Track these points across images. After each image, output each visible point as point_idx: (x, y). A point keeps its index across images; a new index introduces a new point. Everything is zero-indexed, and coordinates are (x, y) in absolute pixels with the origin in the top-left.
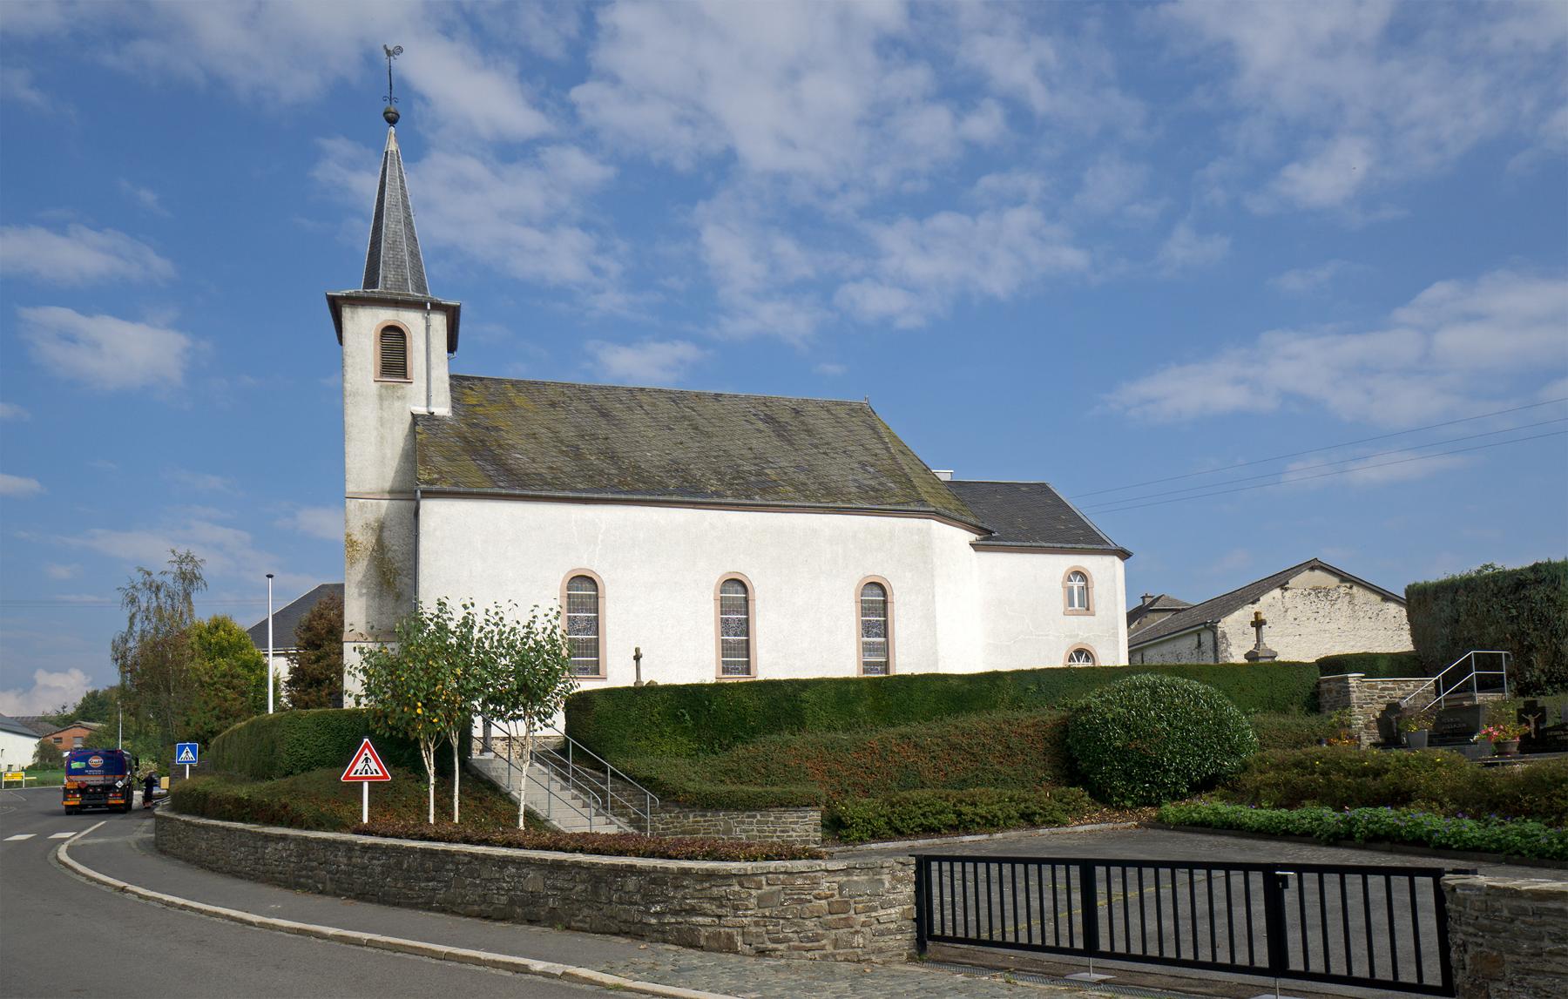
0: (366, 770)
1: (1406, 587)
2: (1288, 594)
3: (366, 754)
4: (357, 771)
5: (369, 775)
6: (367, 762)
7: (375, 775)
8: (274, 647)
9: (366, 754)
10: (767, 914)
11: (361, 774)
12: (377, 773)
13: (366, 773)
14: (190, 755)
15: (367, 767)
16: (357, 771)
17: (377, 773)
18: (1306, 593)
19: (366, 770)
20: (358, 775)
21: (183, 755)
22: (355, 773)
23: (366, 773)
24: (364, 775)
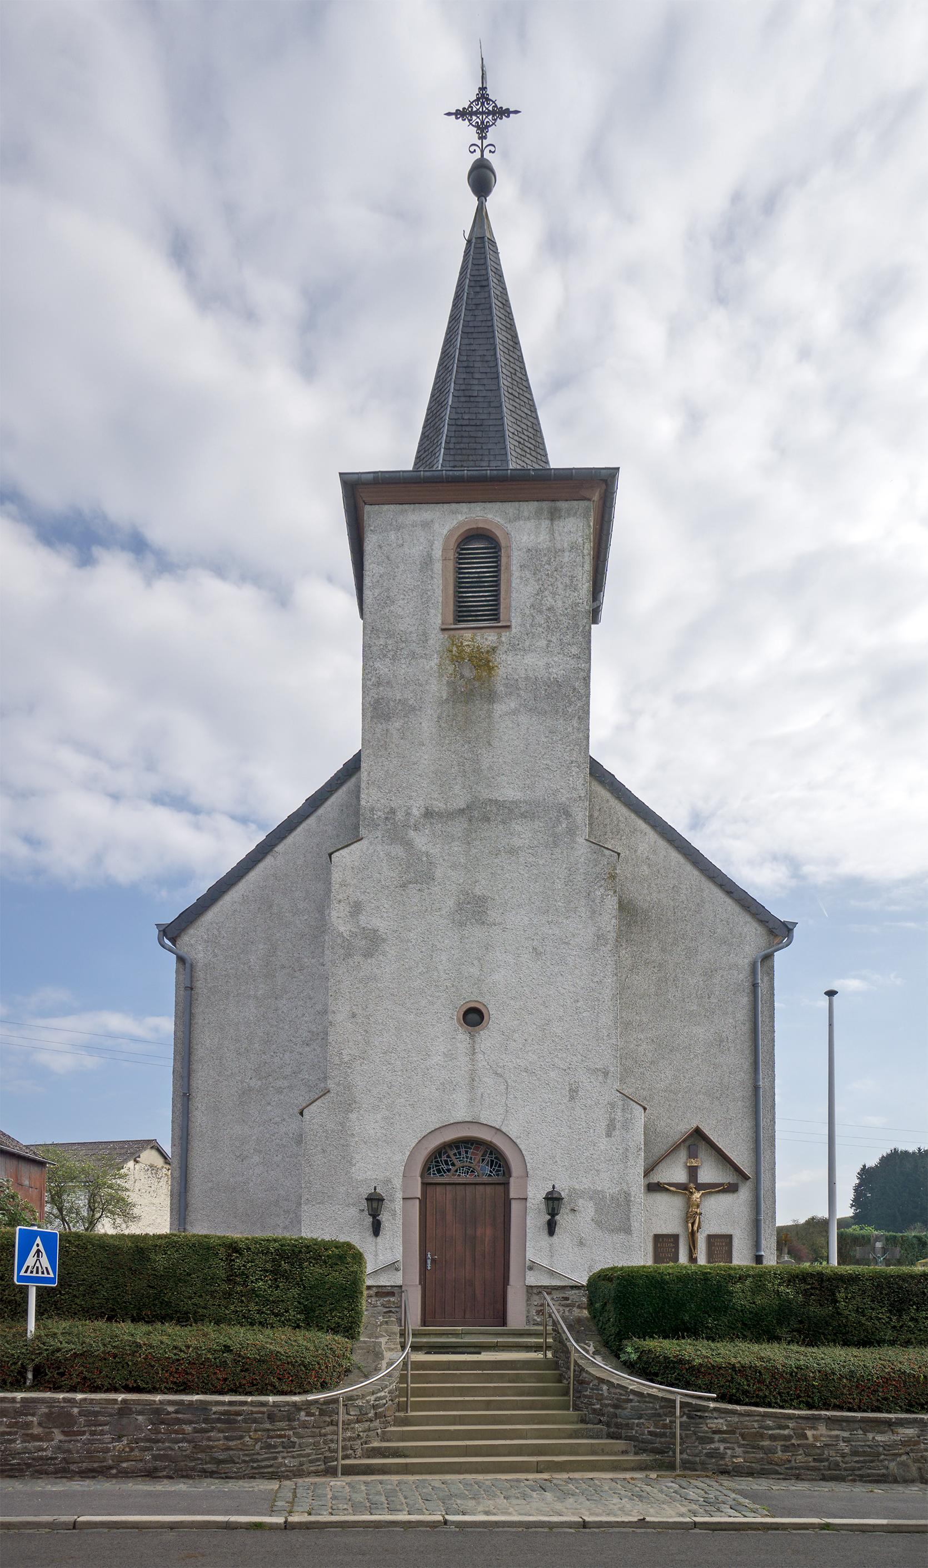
0: (37, 1268)
1: (893, 1148)
2: (137, 1166)
3: (38, 1245)
4: (28, 1267)
5: (40, 1275)
6: (38, 1256)
7: (46, 1275)
8: (40, 1313)
9: (38, 1245)
10: (305, 1342)
11: (32, 1272)
12: (48, 1273)
13: (37, 1272)
14: (45, 1261)
15: (38, 1264)
16: (28, 1267)
17: (48, 1273)
18: (146, 1168)
19: (37, 1268)
20: (28, 1274)
21: (30, 1261)
22: (26, 1272)
23: (37, 1272)
24: (34, 1274)
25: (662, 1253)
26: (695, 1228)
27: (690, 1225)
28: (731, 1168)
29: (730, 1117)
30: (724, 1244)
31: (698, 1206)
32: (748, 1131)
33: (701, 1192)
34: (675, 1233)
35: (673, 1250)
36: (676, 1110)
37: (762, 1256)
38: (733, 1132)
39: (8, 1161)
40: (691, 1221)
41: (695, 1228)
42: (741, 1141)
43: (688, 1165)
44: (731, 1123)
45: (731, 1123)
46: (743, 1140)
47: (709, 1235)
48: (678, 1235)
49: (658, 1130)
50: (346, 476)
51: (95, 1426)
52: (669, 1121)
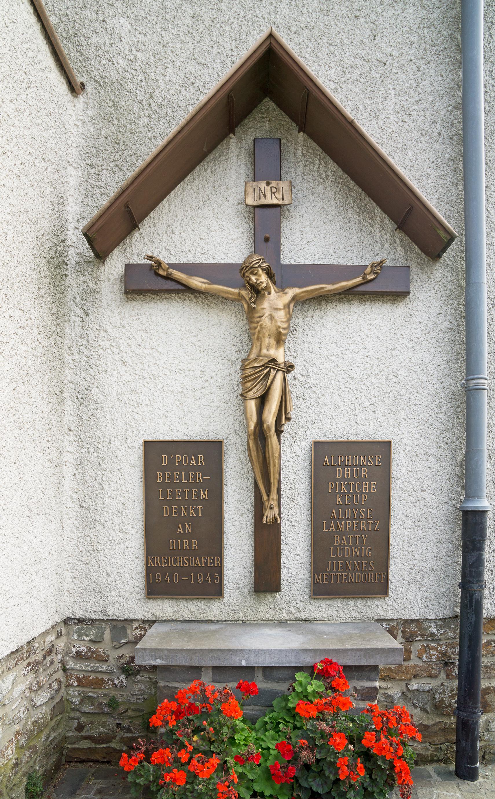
25: (170, 503)
26: (270, 417)
27: (252, 405)
28: (387, 221)
29: (379, 55)
30: (365, 473)
31: (279, 339)
32: (438, 104)
33: (291, 292)
34: (212, 437)
35: (204, 495)
36: (215, 33)
37: (483, 513)
38: (390, 105)
39: (143, 547)
40: (257, 391)
41: (270, 417)
42: (415, 134)
43: (250, 201)
44: (384, 77)
45: (384, 77)
46: (423, 133)
47: (317, 444)
48: (221, 443)
49: (157, 96)
50: (364, 143)
51: (459, 665)
52: (193, 68)
